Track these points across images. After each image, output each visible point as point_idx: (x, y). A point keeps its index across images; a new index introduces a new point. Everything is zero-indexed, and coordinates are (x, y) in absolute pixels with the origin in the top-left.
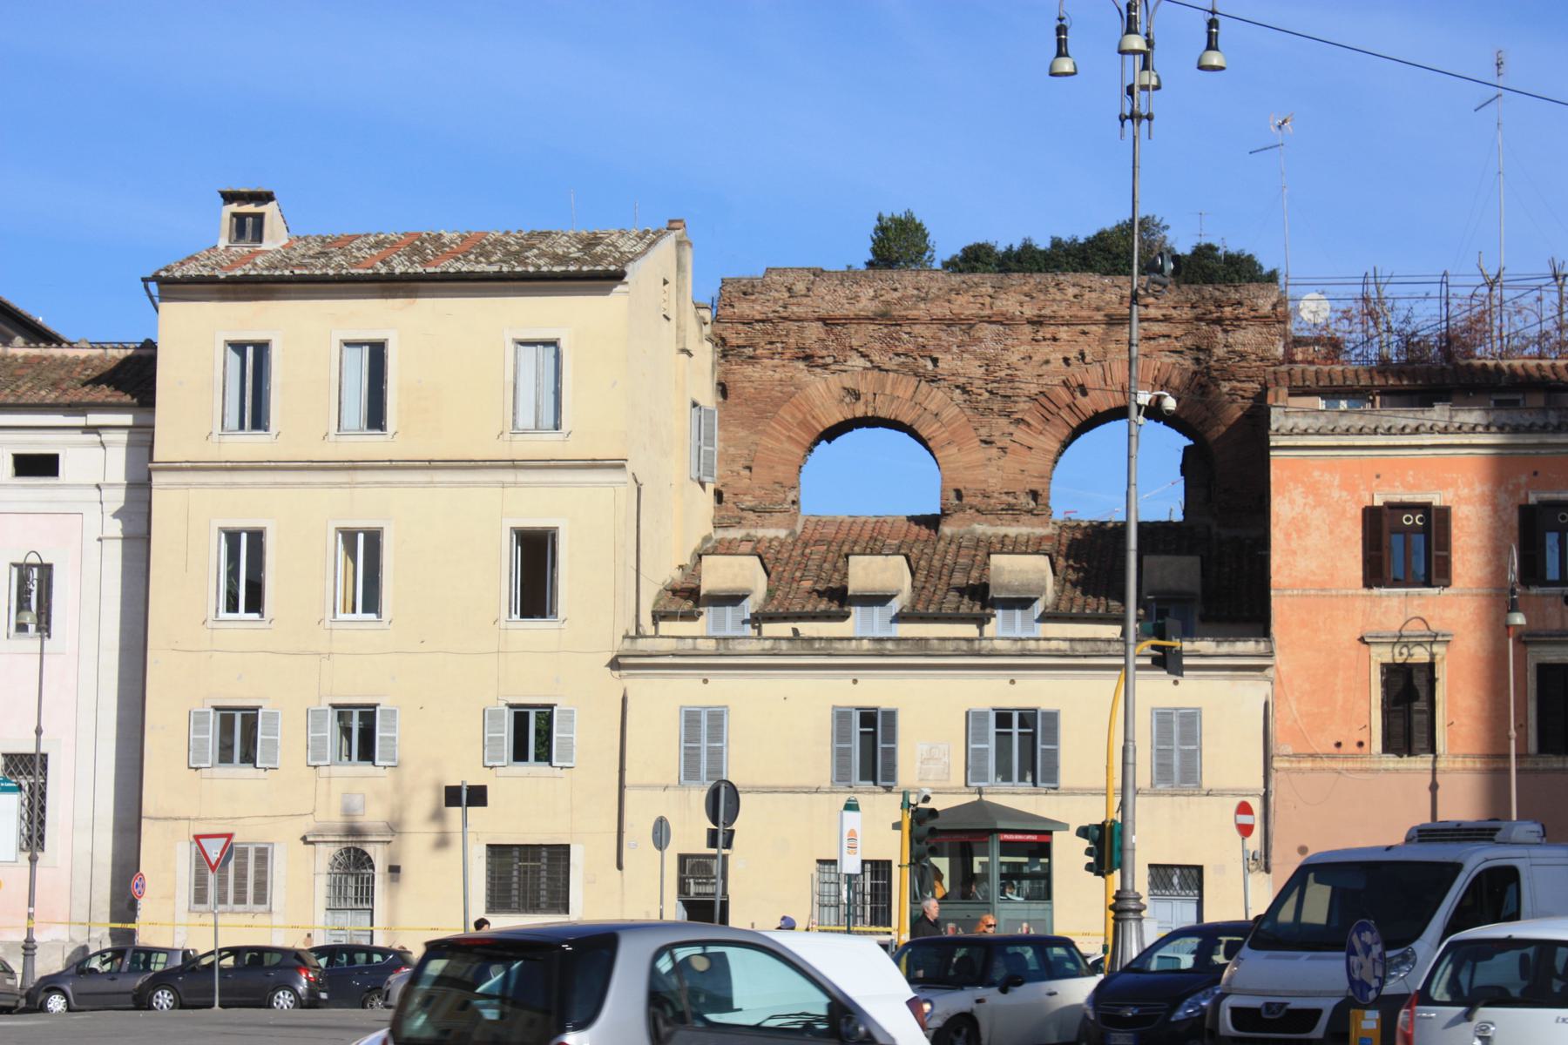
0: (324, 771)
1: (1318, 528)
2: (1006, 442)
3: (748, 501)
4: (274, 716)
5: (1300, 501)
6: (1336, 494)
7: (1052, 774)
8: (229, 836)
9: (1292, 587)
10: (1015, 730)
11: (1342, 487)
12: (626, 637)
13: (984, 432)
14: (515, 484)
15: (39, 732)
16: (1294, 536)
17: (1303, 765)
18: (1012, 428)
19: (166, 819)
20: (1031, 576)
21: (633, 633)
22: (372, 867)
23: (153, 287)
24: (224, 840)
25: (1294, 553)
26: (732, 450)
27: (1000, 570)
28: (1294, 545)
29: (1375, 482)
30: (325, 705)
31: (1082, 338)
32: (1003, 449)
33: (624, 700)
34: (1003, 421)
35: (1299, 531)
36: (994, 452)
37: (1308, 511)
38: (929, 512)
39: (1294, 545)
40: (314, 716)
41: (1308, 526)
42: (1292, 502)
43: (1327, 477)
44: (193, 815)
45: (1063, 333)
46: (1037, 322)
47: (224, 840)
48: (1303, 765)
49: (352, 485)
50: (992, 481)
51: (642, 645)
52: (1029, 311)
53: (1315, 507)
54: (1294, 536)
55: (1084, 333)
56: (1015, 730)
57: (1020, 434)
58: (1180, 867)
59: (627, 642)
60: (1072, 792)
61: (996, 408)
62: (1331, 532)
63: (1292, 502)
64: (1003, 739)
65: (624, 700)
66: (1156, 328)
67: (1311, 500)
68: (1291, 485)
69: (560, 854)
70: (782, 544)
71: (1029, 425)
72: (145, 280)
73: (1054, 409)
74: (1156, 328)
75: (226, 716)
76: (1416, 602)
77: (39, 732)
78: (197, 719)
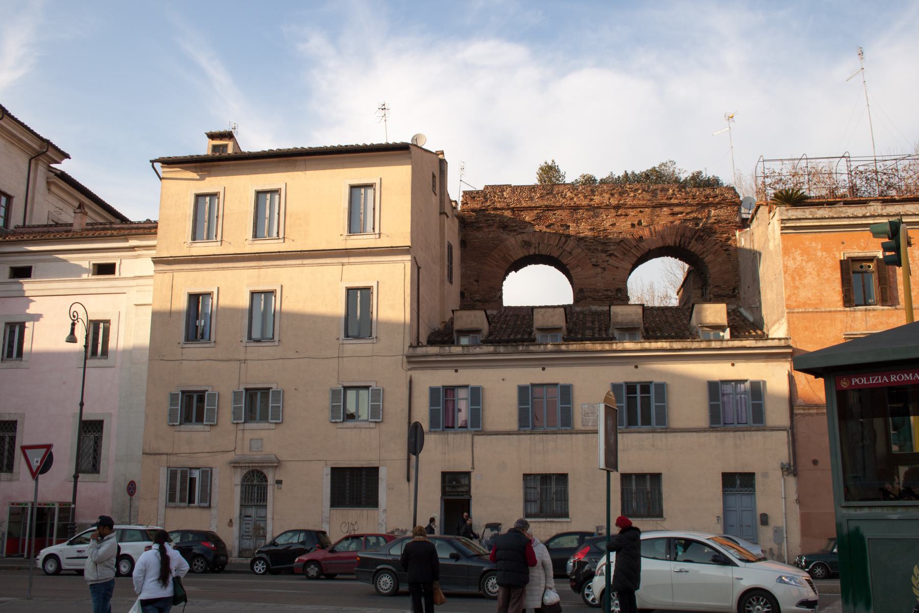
0: (241, 427)
1: (810, 273)
2: (605, 265)
3: (478, 297)
4: (213, 396)
5: (799, 258)
6: (819, 254)
7: (662, 418)
8: (49, 447)
9: (799, 307)
10: (639, 395)
11: (822, 250)
12: (411, 346)
13: (594, 260)
14: (349, 263)
15: (82, 404)
16: (797, 278)
17: (811, 411)
18: (608, 258)
19: (155, 454)
20: (633, 317)
21: (415, 344)
22: (266, 481)
23: (158, 166)
24: (27, 451)
25: (797, 288)
26: (469, 272)
27: (616, 314)
28: (797, 283)
29: (842, 246)
30: (242, 389)
31: (640, 214)
32: (604, 269)
33: (411, 382)
34: (603, 255)
35: (800, 275)
36: (599, 270)
37: (804, 264)
38: (566, 303)
39: (797, 283)
40: (236, 394)
41: (805, 272)
42: (794, 259)
43: (814, 244)
44: (170, 452)
45: (632, 213)
46: (617, 207)
47: (27, 451)
48: (811, 411)
49: (260, 267)
50: (599, 284)
51: (420, 351)
52: (614, 202)
53: (807, 262)
54: (797, 278)
55: (641, 212)
56: (639, 395)
57: (612, 261)
58: (740, 474)
59: (411, 349)
60: (675, 431)
61: (599, 249)
62: (818, 276)
63: (794, 259)
64: (631, 402)
65: (411, 382)
66: (676, 209)
67: (805, 257)
68: (794, 249)
69: (372, 473)
70: (494, 316)
71: (616, 256)
72: (153, 162)
73: (627, 248)
74: (676, 209)
75: (188, 395)
76: (871, 314)
77: (82, 404)
78: (173, 397)
